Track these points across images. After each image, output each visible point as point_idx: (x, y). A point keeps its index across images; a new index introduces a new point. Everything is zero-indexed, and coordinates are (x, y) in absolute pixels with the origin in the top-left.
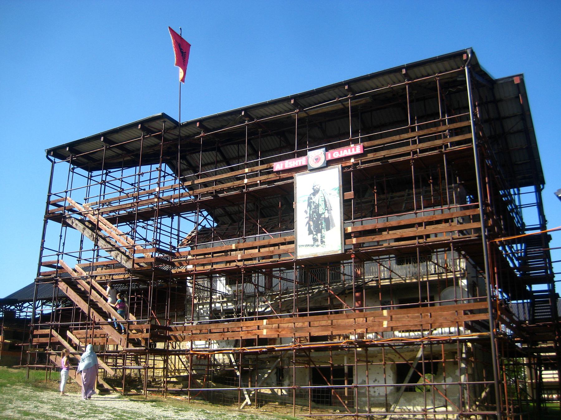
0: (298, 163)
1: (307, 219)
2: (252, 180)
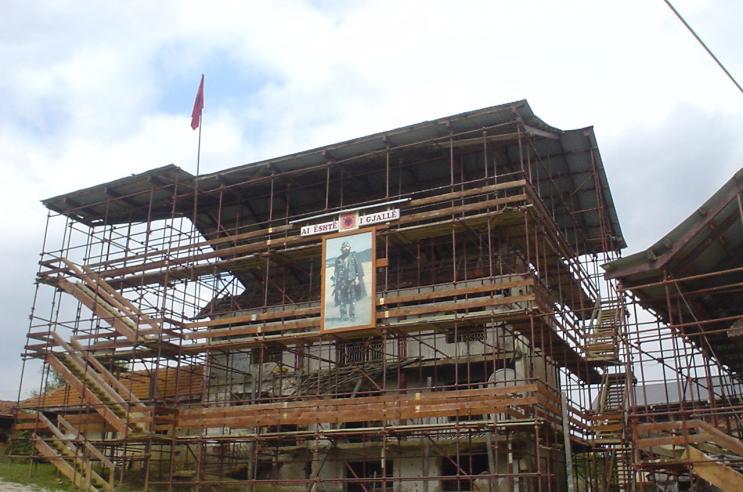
1: (333, 288)
2: (276, 241)
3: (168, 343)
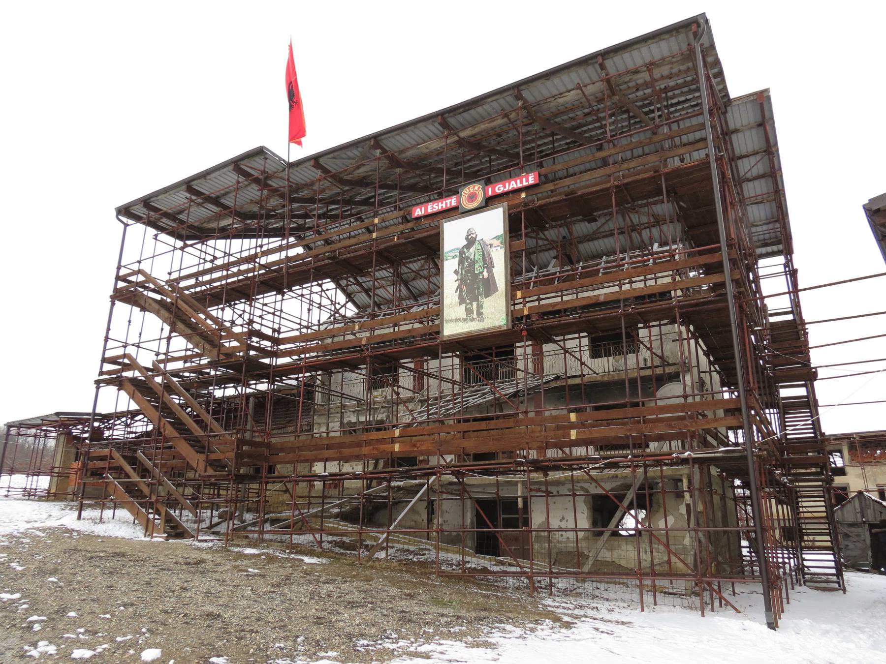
0: (446, 203)
1: (457, 283)
3: (196, 293)
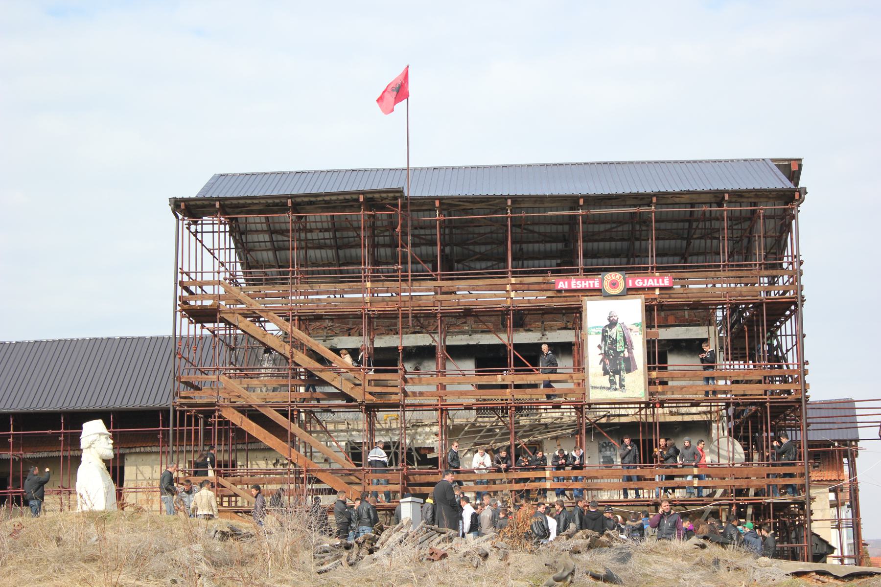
1: (601, 357)
